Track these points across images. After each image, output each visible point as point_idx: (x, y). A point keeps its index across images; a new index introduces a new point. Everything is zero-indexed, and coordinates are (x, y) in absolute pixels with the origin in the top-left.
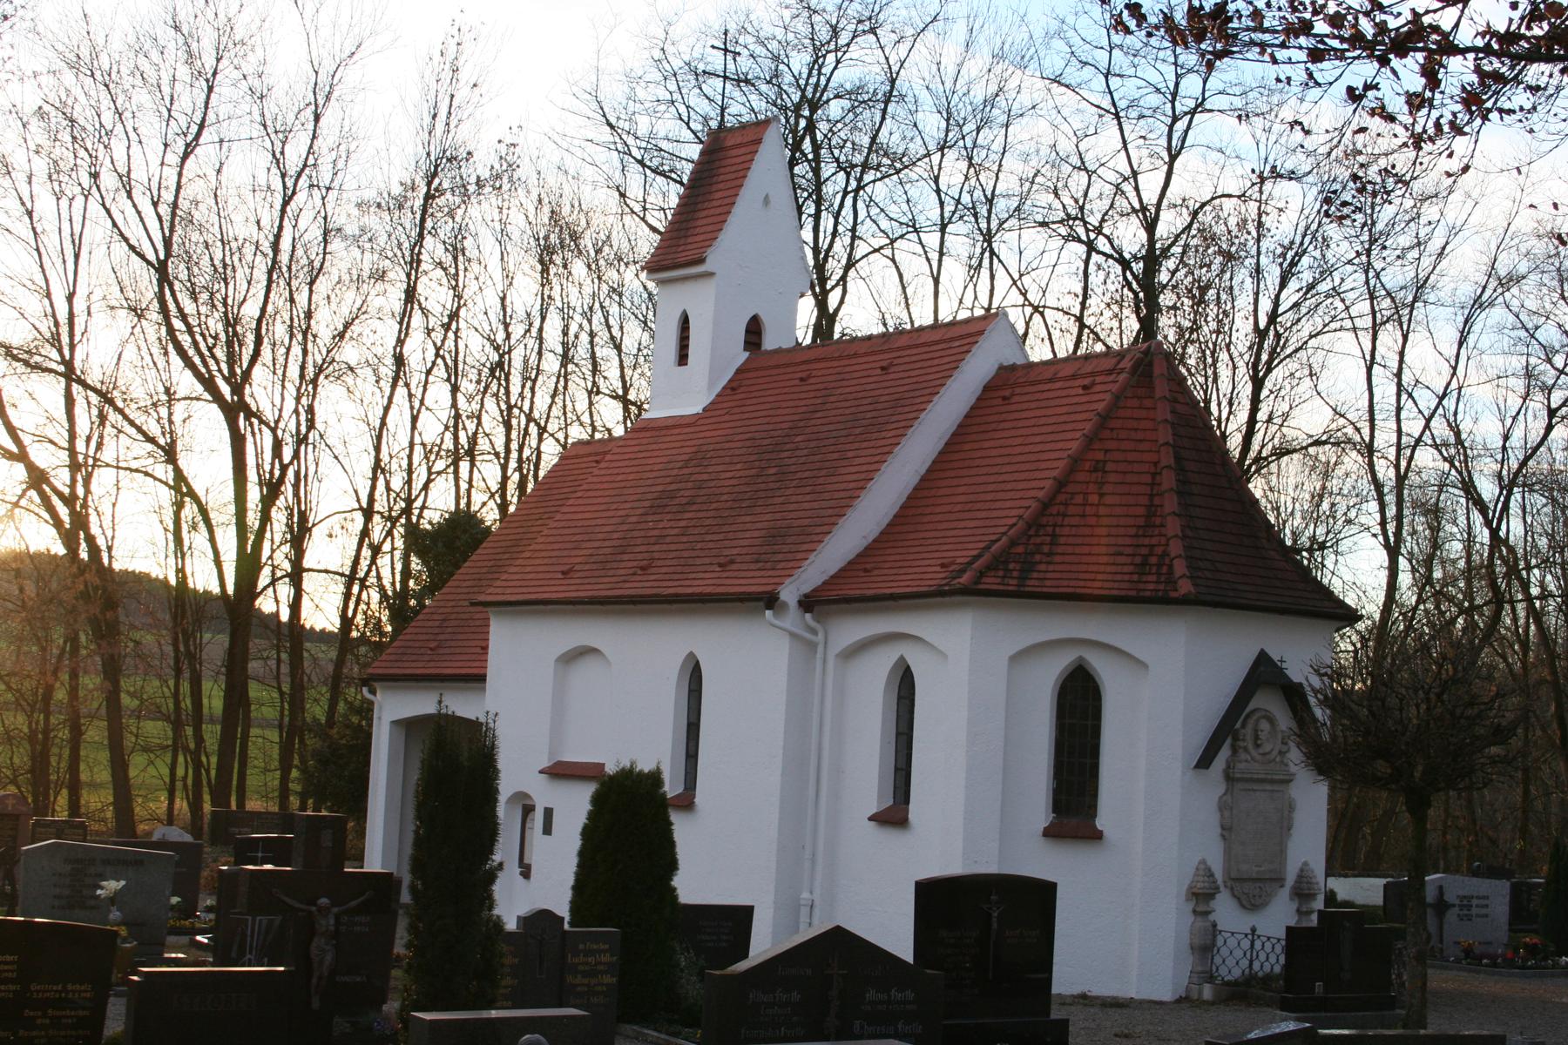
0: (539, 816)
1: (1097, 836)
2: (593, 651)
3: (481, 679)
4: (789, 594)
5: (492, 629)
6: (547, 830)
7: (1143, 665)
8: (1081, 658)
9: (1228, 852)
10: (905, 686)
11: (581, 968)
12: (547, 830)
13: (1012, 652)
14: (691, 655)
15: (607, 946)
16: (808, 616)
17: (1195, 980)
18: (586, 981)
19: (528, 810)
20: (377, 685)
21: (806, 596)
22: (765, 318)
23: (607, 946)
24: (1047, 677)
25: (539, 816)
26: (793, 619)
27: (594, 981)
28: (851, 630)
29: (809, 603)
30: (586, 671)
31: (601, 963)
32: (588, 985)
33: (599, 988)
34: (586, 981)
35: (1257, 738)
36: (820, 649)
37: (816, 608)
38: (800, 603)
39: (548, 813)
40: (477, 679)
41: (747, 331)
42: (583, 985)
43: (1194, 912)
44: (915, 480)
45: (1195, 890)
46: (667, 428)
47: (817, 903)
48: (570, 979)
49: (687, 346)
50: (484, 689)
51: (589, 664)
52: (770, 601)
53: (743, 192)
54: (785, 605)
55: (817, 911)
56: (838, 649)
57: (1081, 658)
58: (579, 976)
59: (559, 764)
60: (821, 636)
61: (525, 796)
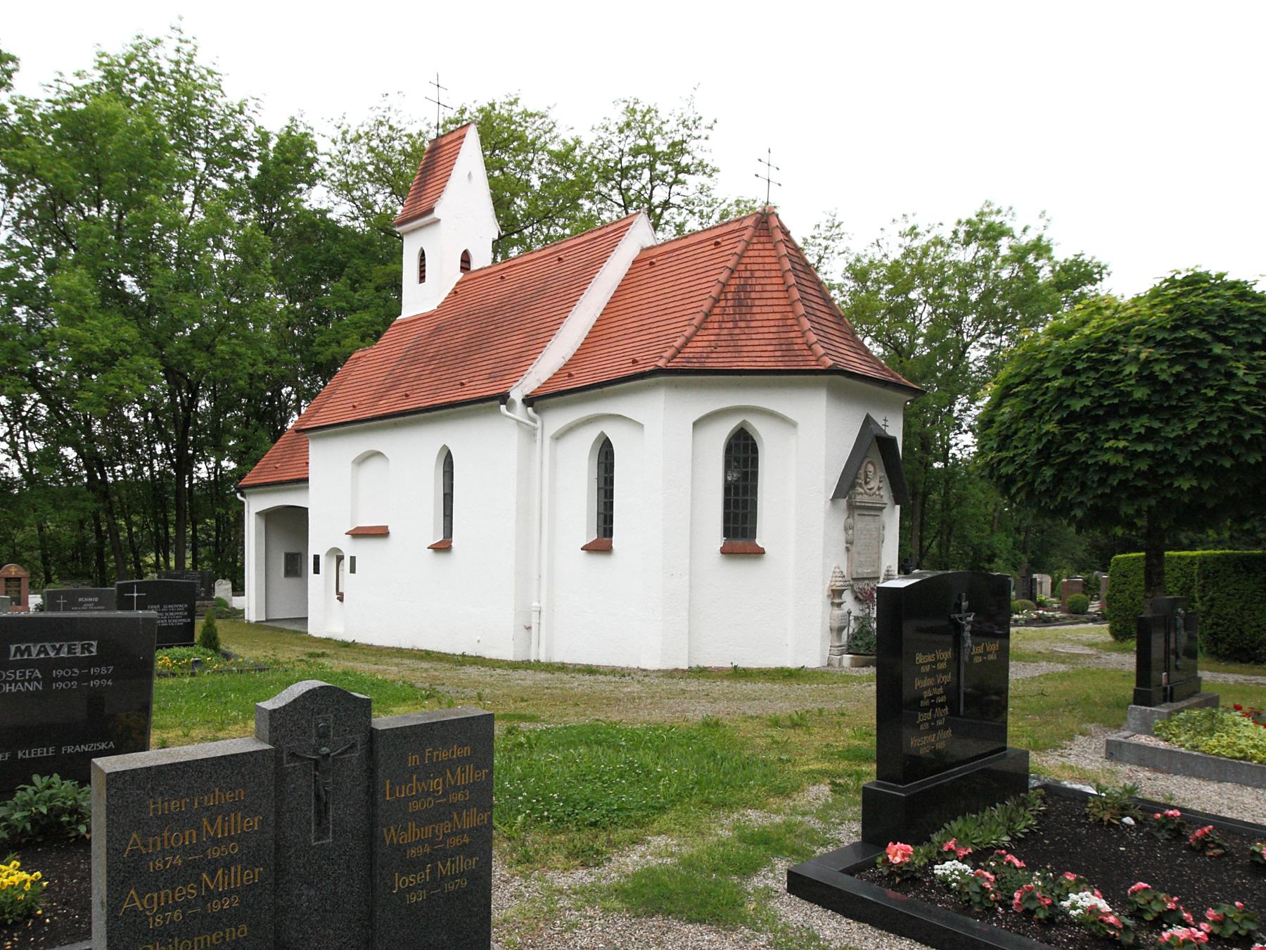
0: (347, 562)
1: (760, 552)
2: (378, 454)
3: (306, 480)
4: (517, 395)
5: (310, 453)
6: (353, 570)
7: (792, 424)
8: (744, 422)
9: (850, 560)
10: (605, 454)
11: (414, 806)
12: (353, 570)
13: (695, 419)
14: (445, 446)
15: (467, 751)
16: (530, 409)
17: (835, 651)
18: (427, 832)
19: (340, 559)
20: (245, 491)
21: (527, 396)
22: (471, 252)
23: (467, 751)
24: (720, 434)
25: (347, 562)
26: (520, 412)
27: (444, 828)
28: (557, 419)
29: (529, 401)
30: (374, 465)
31: (456, 788)
32: (431, 842)
33: (456, 841)
34: (427, 832)
35: (866, 476)
36: (539, 433)
37: (536, 403)
38: (524, 401)
39: (353, 559)
40: (302, 482)
41: (462, 261)
42: (420, 842)
43: (833, 604)
44: (593, 321)
45: (834, 588)
46: (411, 322)
47: (544, 609)
48: (390, 835)
49: (424, 271)
50: (308, 487)
51: (374, 464)
52: (504, 398)
53: (455, 167)
54: (513, 402)
55: (543, 614)
56: (554, 431)
57: (744, 422)
58: (412, 825)
59: (358, 528)
60: (539, 424)
61: (339, 550)
